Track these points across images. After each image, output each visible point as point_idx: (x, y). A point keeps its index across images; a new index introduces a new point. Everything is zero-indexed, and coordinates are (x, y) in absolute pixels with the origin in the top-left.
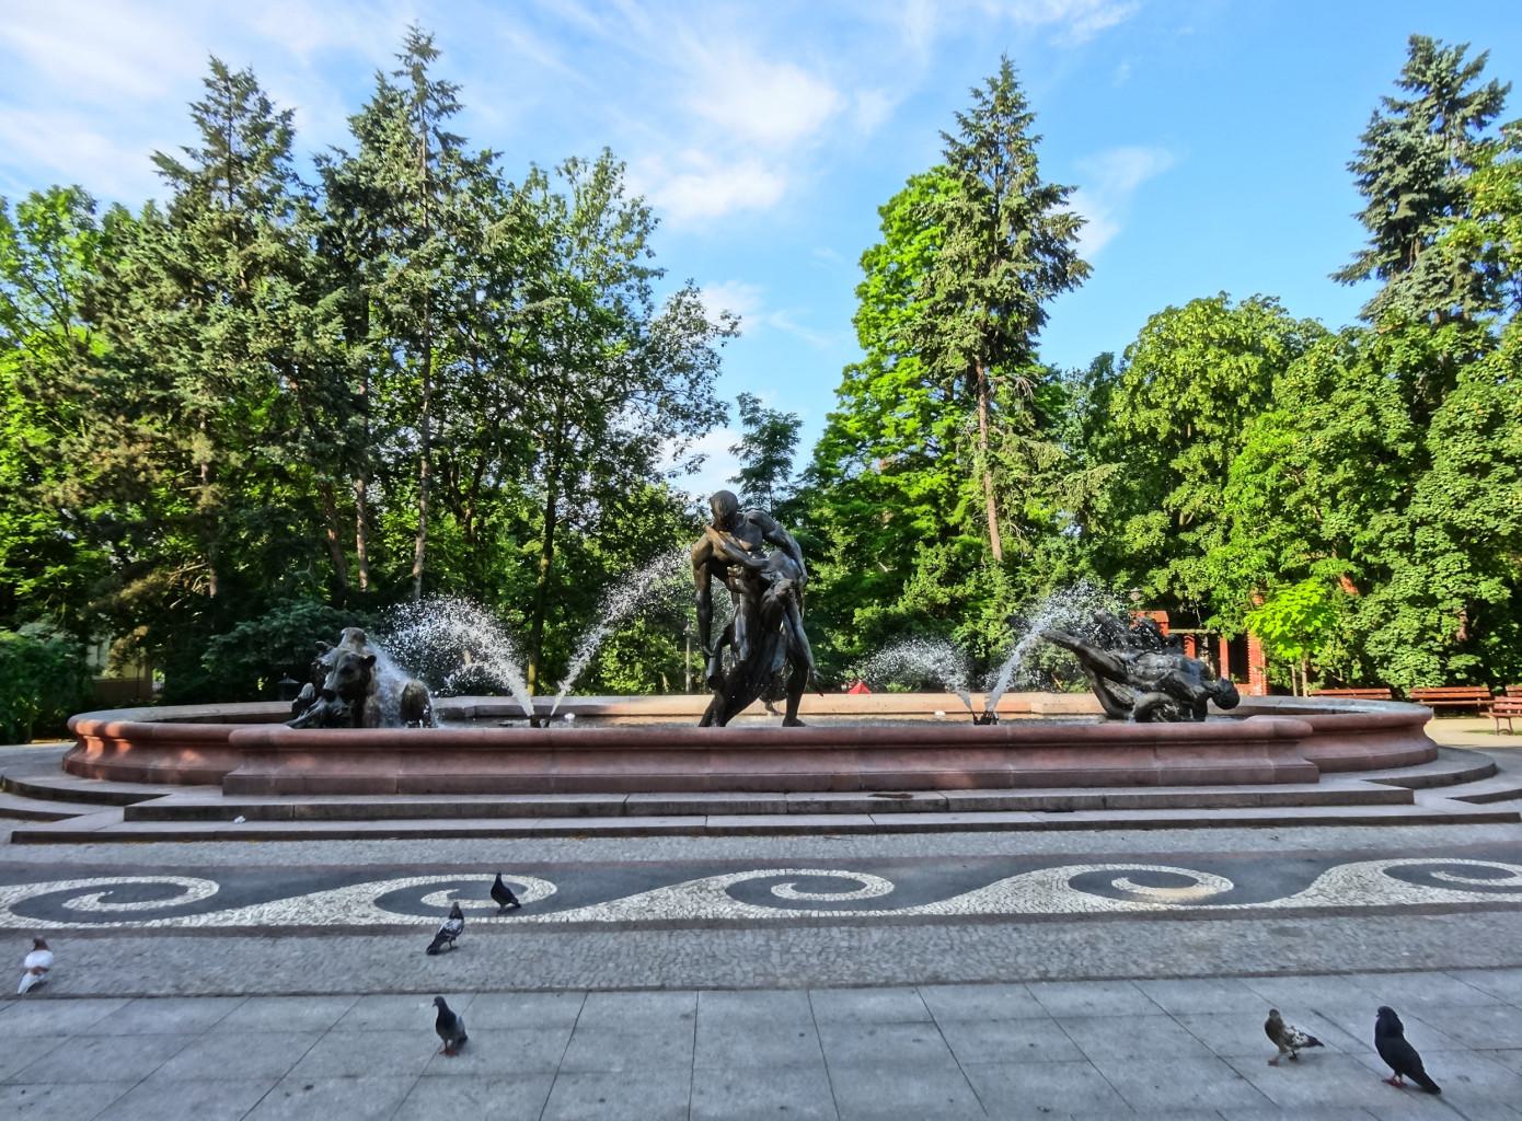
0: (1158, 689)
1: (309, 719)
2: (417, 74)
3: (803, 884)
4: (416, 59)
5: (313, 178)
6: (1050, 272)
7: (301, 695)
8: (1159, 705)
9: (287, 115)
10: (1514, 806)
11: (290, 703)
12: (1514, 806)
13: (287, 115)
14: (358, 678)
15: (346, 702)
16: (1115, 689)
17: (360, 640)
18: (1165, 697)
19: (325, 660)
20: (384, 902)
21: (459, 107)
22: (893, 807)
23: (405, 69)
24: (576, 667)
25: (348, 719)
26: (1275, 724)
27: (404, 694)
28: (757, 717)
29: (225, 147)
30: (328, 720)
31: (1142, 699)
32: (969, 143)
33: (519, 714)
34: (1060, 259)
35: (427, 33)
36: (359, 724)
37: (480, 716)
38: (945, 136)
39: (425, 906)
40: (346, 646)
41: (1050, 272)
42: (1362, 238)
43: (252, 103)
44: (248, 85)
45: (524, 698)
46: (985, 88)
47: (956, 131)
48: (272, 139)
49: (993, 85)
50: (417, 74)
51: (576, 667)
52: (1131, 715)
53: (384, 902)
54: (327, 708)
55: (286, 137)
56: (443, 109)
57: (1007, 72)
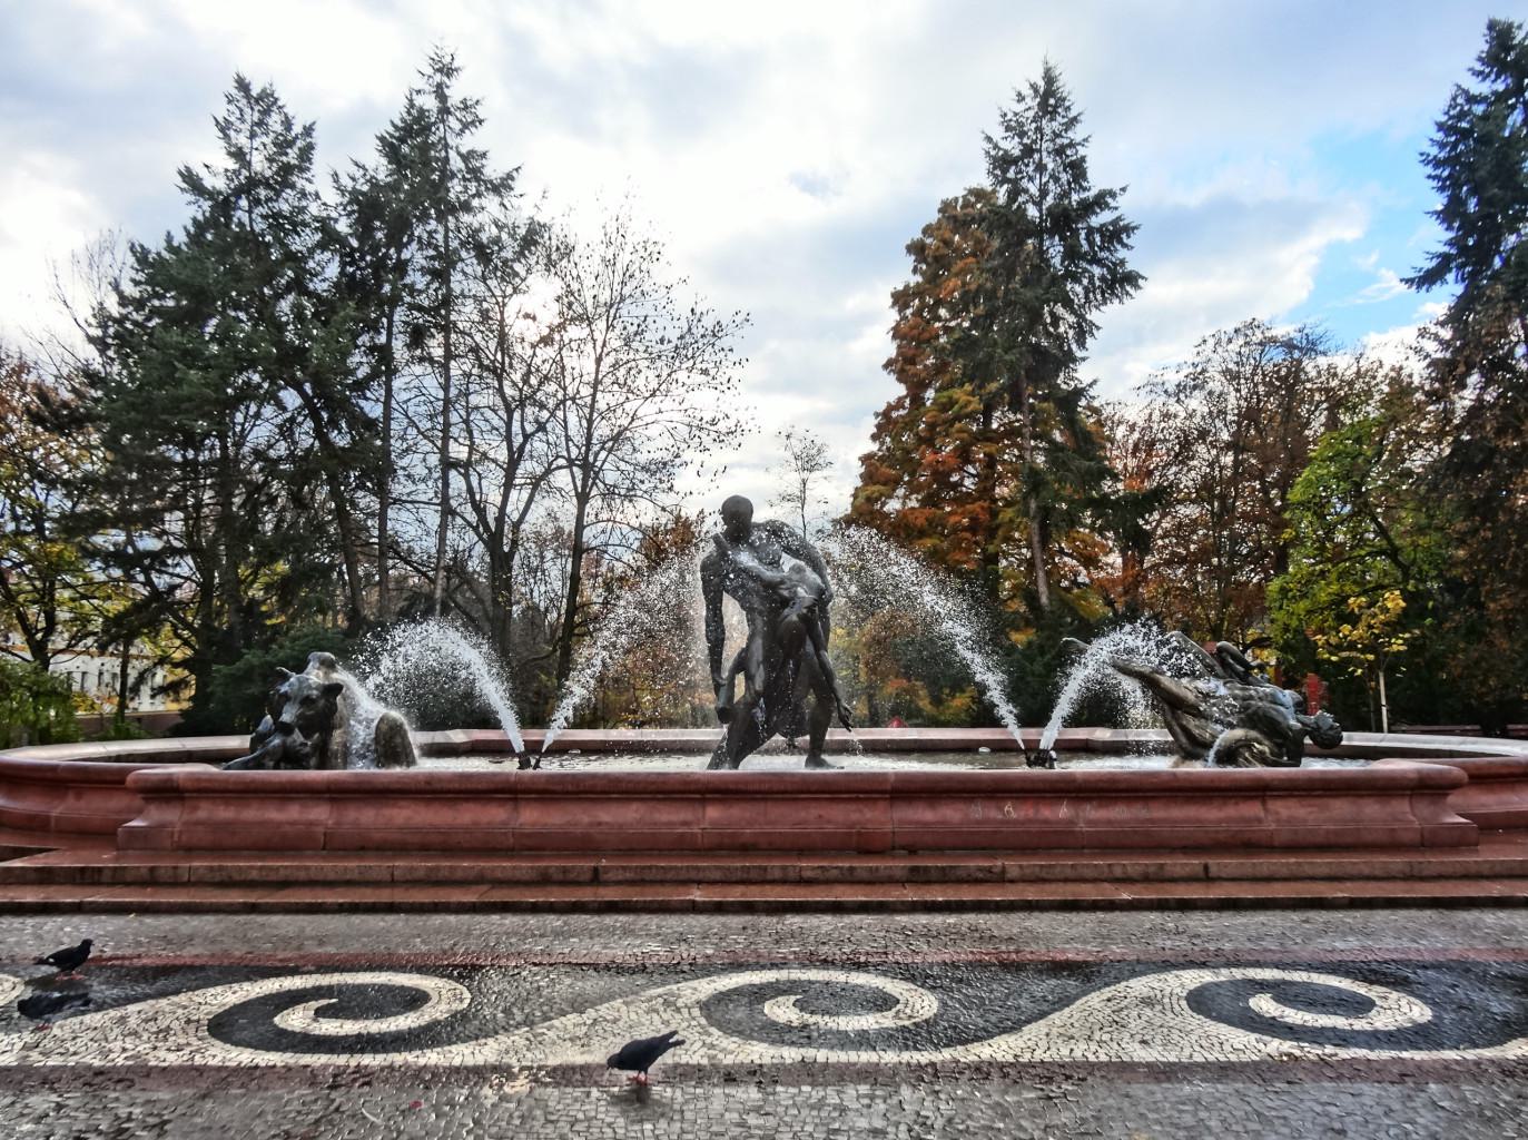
0: (1243, 724)
1: (262, 756)
2: (440, 93)
3: (807, 997)
4: (438, 77)
5: (331, 197)
6: (1098, 283)
7: (260, 728)
8: (1247, 744)
9: (308, 131)
10: (1516, 801)
11: (249, 737)
12: (1516, 801)
13: (308, 131)
14: (324, 711)
15: (307, 736)
16: (1192, 723)
17: (329, 666)
18: (1253, 734)
19: (284, 688)
20: (222, 1027)
21: (481, 122)
22: (934, 875)
23: (427, 88)
24: (578, 690)
25: (307, 756)
26: (1419, 771)
27: (378, 727)
28: (775, 761)
29: (247, 165)
30: (291, 758)
31: (1227, 736)
32: (1013, 146)
33: (501, 750)
34: (1109, 268)
35: (449, 51)
36: (322, 766)
37: (474, 750)
38: (989, 139)
39: (283, 1033)
40: (315, 676)
41: (1098, 283)
42: (1437, 238)
43: (275, 121)
44: (266, 102)
45: (515, 735)
46: (1027, 92)
47: (998, 133)
48: (292, 156)
49: (1034, 87)
50: (440, 93)
51: (578, 690)
52: (1212, 753)
53: (222, 1027)
54: (284, 743)
55: (306, 154)
56: (465, 126)
57: (1050, 79)
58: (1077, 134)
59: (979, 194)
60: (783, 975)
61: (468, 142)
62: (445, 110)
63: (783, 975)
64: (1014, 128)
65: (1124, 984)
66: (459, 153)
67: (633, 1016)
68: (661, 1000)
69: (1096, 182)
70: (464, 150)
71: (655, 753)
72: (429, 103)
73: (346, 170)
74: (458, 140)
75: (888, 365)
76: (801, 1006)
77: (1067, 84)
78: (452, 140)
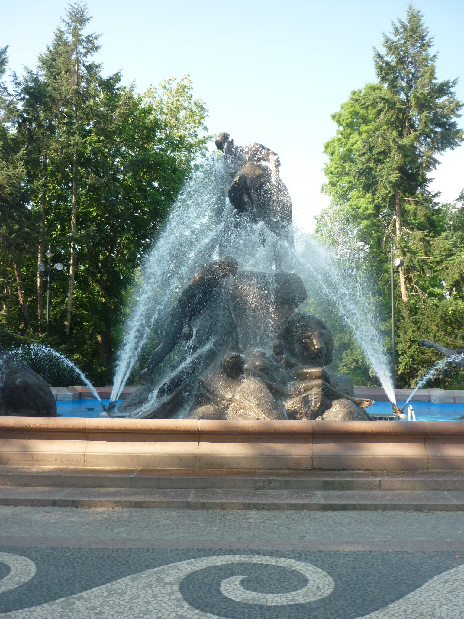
2: (76, 34)
47: (383, 51)
56: (88, 51)
57: (414, 31)
58: (431, 52)
59: (374, 88)
60: (237, 559)
61: (89, 60)
62: (78, 41)
63: (237, 559)
64: (392, 48)
65: (455, 569)
66: (84, 65)
67: (135, 590)
68: (155, 577)
69: (440, 78)
70: (87, 64)
71: (380, 293)
72: (70, 38)
73: (22, 76)
74: (84, 59)
75: (324, 187)
76: (246, 584)
77: (431, 25)
78: (83, 59)
